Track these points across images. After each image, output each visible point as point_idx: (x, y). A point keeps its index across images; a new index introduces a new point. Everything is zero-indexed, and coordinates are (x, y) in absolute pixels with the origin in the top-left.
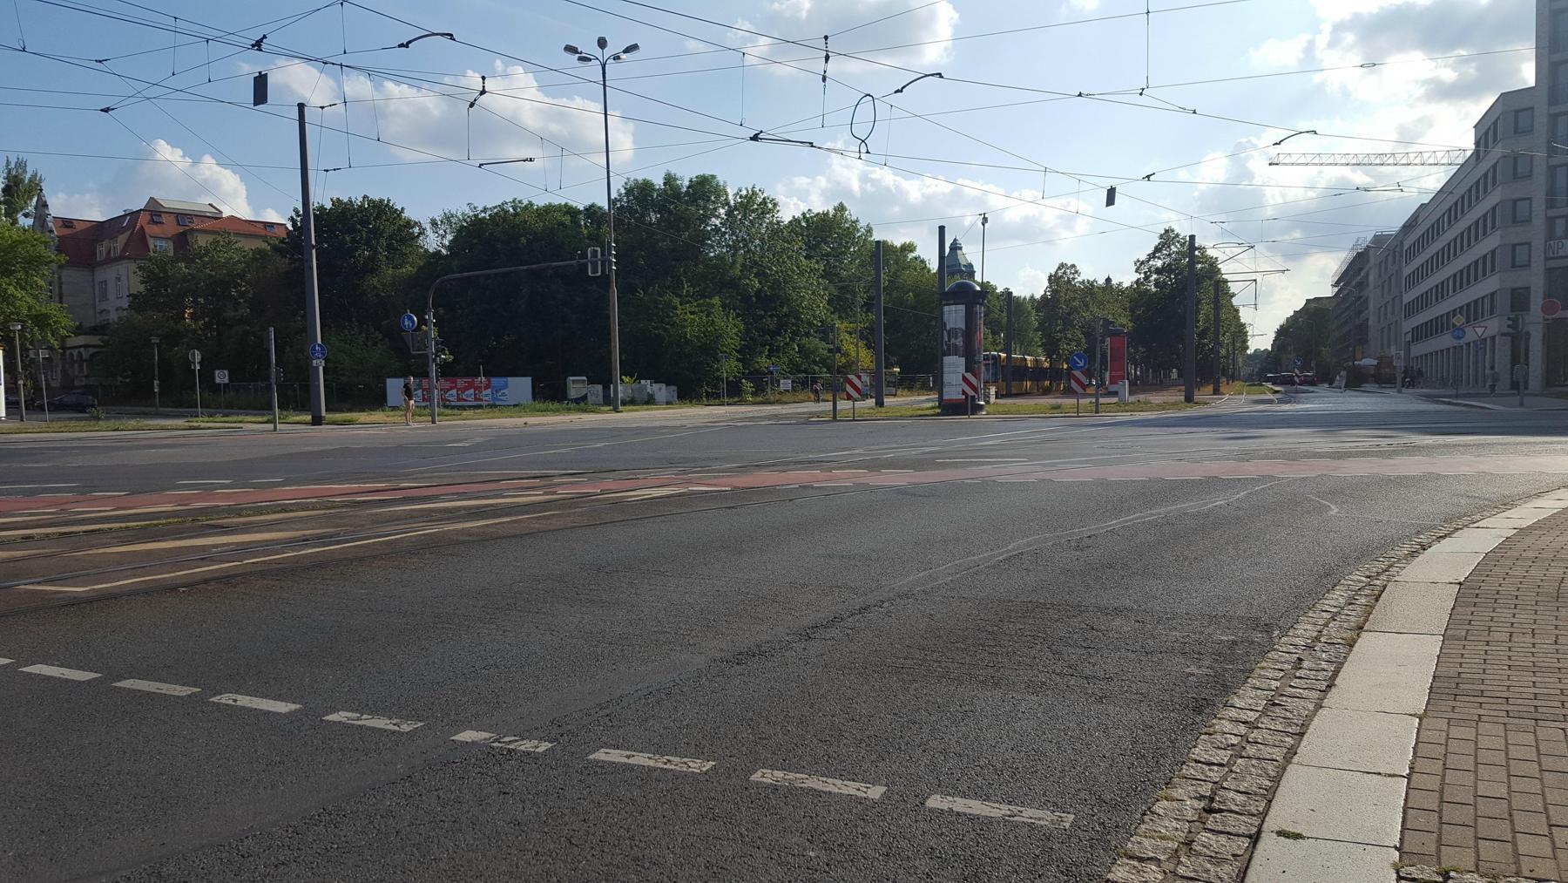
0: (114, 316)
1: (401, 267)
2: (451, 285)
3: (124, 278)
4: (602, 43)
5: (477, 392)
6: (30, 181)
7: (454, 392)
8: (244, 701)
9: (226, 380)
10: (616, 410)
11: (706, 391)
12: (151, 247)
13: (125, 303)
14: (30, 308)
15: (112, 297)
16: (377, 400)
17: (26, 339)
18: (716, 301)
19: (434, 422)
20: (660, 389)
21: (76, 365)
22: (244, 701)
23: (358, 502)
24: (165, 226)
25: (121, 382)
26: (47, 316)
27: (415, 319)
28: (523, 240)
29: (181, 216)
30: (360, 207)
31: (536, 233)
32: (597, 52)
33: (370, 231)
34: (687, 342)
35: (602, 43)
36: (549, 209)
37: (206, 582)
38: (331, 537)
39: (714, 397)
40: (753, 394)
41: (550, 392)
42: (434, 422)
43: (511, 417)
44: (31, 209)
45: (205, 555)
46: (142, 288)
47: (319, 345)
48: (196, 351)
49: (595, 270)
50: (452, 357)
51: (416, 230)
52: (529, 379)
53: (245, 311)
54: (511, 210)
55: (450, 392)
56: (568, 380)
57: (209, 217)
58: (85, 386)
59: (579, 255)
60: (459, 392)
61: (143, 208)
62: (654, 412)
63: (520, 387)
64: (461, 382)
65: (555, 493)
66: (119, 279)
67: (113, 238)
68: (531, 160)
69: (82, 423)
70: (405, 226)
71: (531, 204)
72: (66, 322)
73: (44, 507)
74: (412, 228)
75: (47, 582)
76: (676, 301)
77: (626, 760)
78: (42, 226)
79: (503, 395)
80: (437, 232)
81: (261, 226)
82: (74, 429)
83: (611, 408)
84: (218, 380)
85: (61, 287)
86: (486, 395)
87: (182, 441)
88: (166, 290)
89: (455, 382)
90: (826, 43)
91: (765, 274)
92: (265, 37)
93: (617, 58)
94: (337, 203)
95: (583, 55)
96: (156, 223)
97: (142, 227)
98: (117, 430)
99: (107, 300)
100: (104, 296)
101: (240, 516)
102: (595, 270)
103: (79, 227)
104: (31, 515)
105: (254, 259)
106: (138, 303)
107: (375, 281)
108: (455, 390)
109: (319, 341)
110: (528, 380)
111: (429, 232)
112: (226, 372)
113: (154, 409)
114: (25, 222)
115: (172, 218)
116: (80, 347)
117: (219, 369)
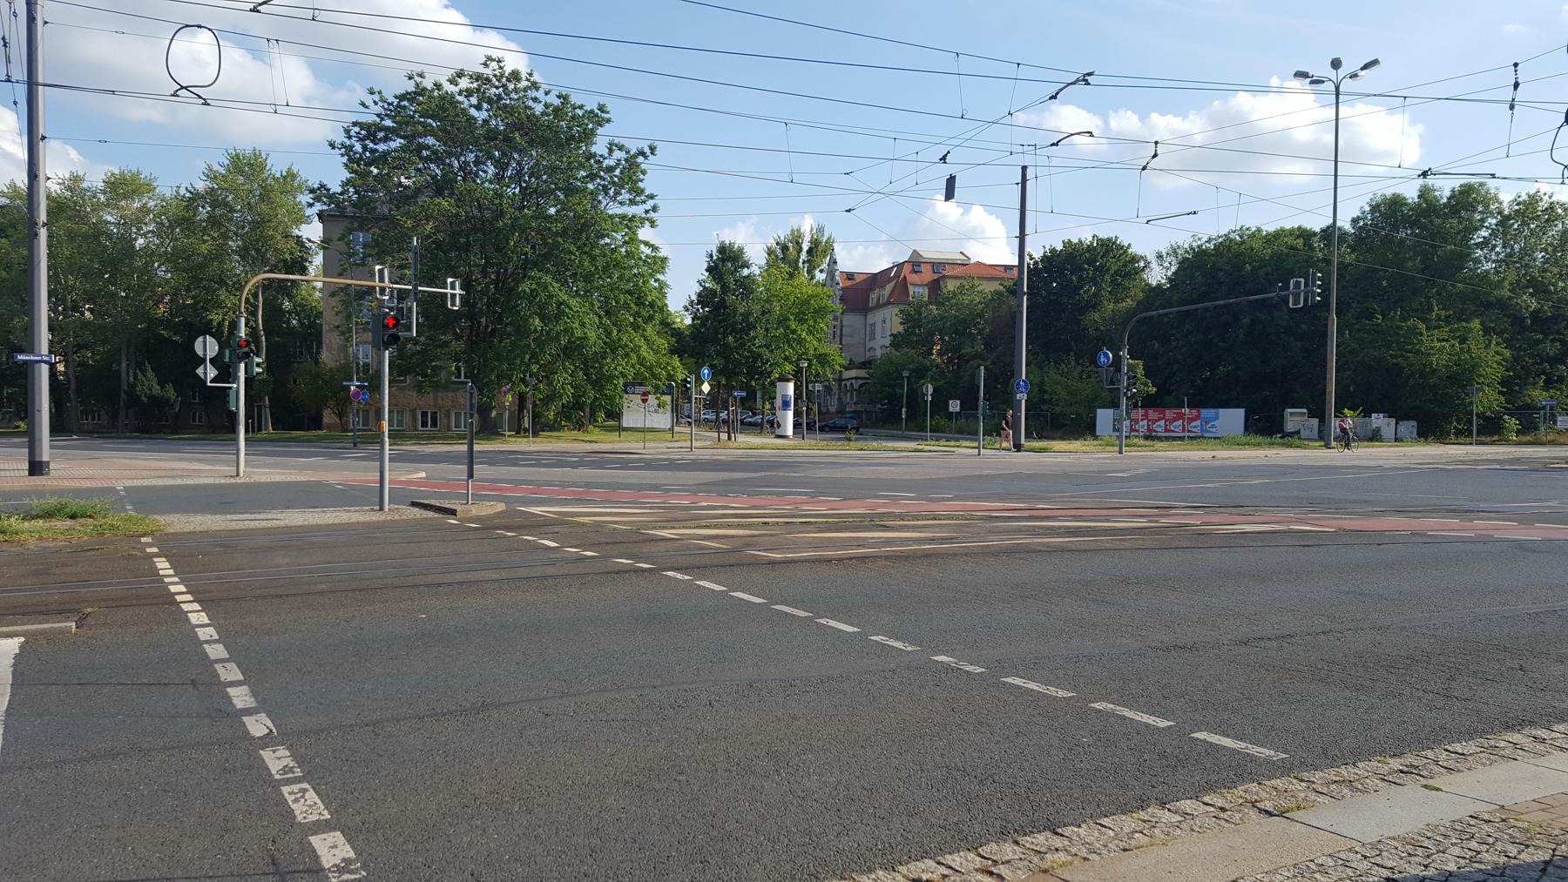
0: (878, 353)
1: (1123, 301)
2: (1169, 318)
3: (888, 321)
4: (1336, 64)
5: (1167, 423)
6: (826, 242)
7: (1162, 423)
8: (832, 623)
9: (958, 409)
10: (1328, 446)
11: (1455, 428)
12: (911, 293)
13: (887, 341)
14: (816, 349)
15: (878, 336)
16: (1086, 429)
17: (812, 374)
18: (1476, 324)
19: (1121, 452)
20: (1388, 424)
21: (849, 394)
22: (832, 623)
23: (992, 517)
24: (923, 275)
25: (880, 409)
26: (826, 355)
27: (1111, 355)
28: (1248, 267)
29: (936, 265)
30: (1089, 246)
31: (1262, 260)
32: (1331, 73)
33: (1096, 269)
34: (1434, 371)
35: (1336, 64)
36: (1278, 235)
37: (851, 559)
38: (952, 539)
39: (1463, 435)
40: (1518, 432)
41: (1265, 425)
42: (1121, 452)
43: (1205, 450)
44: (824, 266)
45: (862, 543)
46: (901, 329)
47: (1023, 381)
48: (929, 386)
49: (1296, 302)
50: (1155, 389)
51: (1142, 264)
52: (1243, 410)
53: (980, 347)
54: (1238, 238)
55: (1157, 423)
56: (1285, 413)
57: (959, 264)
58: (854, 412)
59: (1280, 287)
60: (1133, 423)
61: (906, 260)
62: (1375, 449)
63: (1232, 419)
64: (1169, 414)
65: (1157, 522)
66: (884, 322)
67: (882, 287)
68: (1195, 213)
69: (840, 443)
70: (1130, 262)
71: (1259, 230)
72: (839, 360)
73: (786, 505)
74: (1137, 262)
75: (765, 550)
76: (1422, 327)
77: (1022, 684)
78: (832, 280)
79: (1213, 426)
80: (1161, 265)
81: (1002, 269)
82: (840, 448)
83: (1323, 443)
84: (951, 409)
85: (841, 330)
86: (1195, 427)
87: (905, 461)
88: (920, 330)
89: (1164, 413)
90: (1516, 71)
91: (1547, 292)
92: (949, 152)
93: (1354, 76)
94: (1067, 244)
95: (1315, 78)
96: (916, 272)
97: (905, 277)
98: (862, 450)
99: (874, 339)
100: (873, 337)
101: (903, 520)
102: (1296, 302)
103: (858, 279)
104: (780, 509)
105: (992, 300)
106: (897, 341)
107: (1097, 316)
108: (1163, 421)
109: (1024, 378)
110: (1240, 413)
111: (1154, 265)
112: (958, 402)
113: (901, 432)
114: (820, 277)
115: (929, 267)
116: (852, 378)
117: (952, 399)
